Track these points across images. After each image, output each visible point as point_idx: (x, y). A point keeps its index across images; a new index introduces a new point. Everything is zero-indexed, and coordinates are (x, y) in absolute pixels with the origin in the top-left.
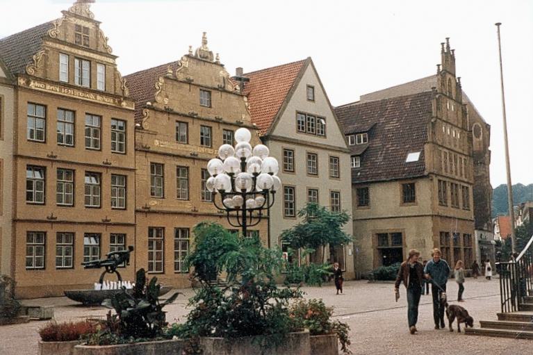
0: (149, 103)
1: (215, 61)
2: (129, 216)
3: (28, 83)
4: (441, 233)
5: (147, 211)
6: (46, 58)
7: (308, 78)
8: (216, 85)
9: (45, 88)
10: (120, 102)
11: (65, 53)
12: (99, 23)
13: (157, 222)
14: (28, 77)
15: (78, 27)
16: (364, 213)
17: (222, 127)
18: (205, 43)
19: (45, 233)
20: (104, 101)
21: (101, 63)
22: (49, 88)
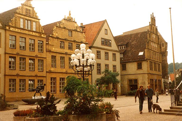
0: (51, 35)
1: (73, 21)
2: (44, 74)
3: (10, 28)
4: (151, 79)
5: (50, 72)
6: (16, 20)
7: (105, 26)
8: (74, 29)
9: (15, 30)
10: (41, 35)
11: (22, 18)
12: (34, 8)
13: (54, 76)
14: (10, 26)
15: (27, 9)
16: (124, 72)
17: (76, 43)
18: (70, 15)
19: (15, 79)
20: (35, 34)
21: (35, 21)
22: (17, 30)
